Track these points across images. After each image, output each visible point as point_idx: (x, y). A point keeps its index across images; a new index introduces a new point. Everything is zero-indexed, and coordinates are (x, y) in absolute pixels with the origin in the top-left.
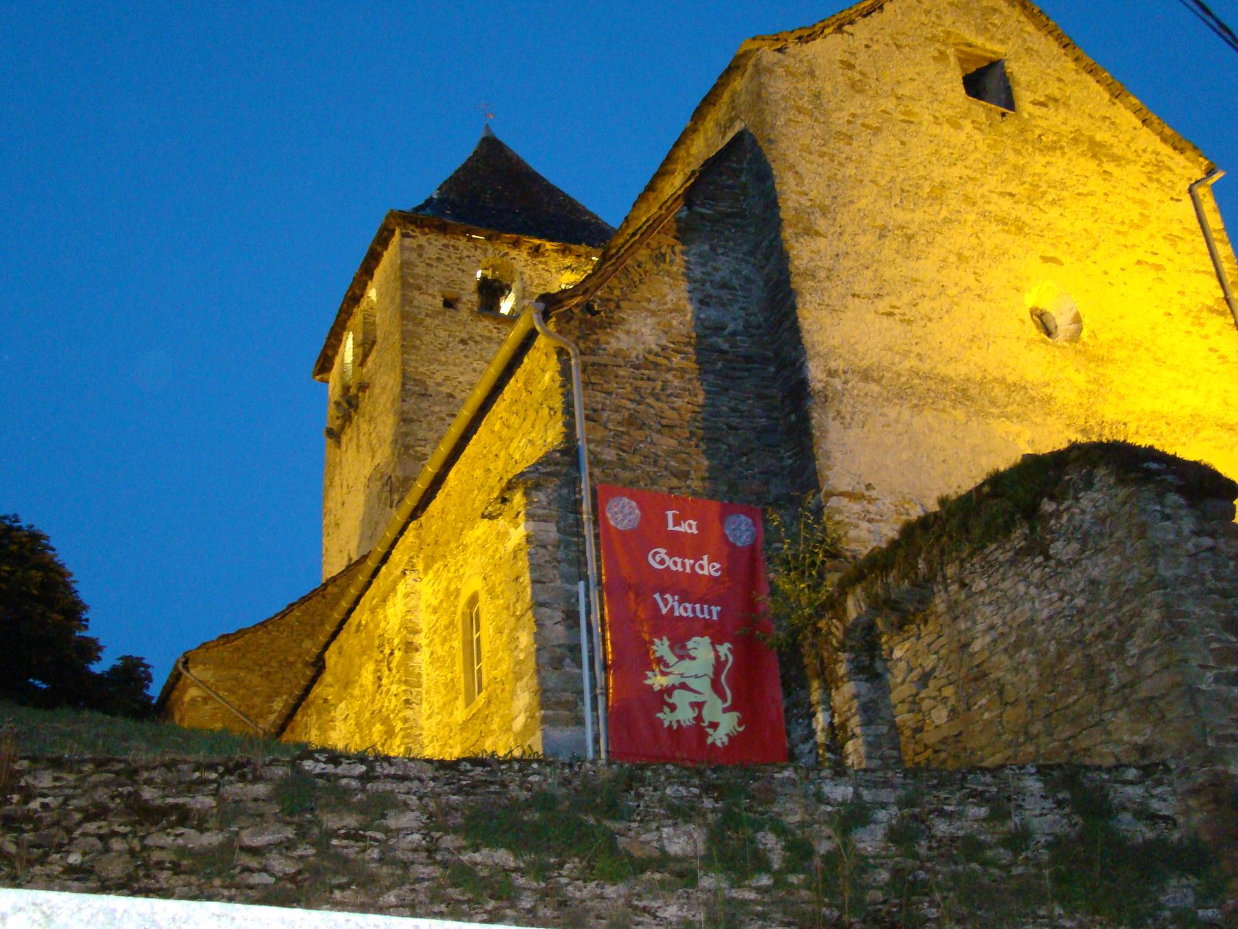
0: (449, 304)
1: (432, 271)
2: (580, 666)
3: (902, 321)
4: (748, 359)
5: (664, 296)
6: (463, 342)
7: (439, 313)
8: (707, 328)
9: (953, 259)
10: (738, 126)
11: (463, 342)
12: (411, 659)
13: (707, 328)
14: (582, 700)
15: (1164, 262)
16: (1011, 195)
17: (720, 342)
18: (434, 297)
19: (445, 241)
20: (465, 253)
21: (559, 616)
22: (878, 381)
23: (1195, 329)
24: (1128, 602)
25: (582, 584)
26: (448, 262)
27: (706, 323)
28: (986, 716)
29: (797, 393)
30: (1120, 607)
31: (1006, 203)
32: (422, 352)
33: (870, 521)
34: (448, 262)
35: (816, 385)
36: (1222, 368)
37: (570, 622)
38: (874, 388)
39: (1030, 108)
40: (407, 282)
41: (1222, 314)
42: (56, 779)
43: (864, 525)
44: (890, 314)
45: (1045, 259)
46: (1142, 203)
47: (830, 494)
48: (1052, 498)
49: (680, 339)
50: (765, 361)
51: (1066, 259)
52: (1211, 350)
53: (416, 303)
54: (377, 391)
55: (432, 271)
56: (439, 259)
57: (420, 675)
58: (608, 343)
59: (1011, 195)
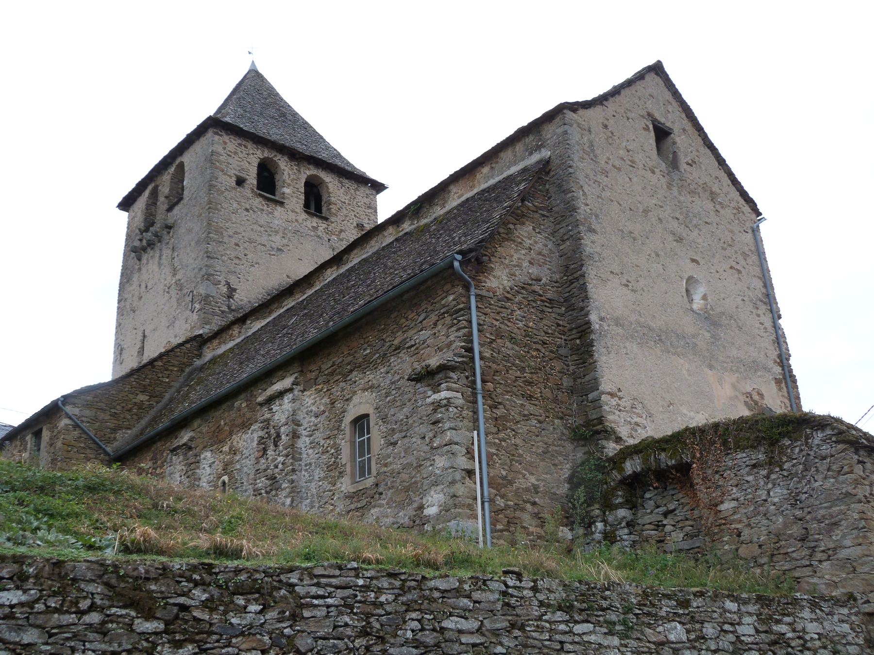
0: (240, 182)
1: (231, 161)
2: (475, 483)
3: (632, 290)
4: (551, 301)
5: (512, 256)
6: (247, 210)
7: (234, 188)
8: (532, 280)
9: (653, 255)
10: (545, 153)
11: (247, 210)
12: (296, 443)
13: (532, 280)
14: (476, 504)
15: (742, 269)
16: (678, 219)
17: (537, 288)
18: (231, 177)
19: (240, 142)
20: (251, 152)
21: (464, 451)
22: (622, 326)
23: (754, 311)
24: (836, 505)
25: (475, 432)
26: (241, 155)
27: (532, 276)
28: (726, 547)
29: (584, 330)
30: (830, 507)
31: (675, 224)
32: (221, 213)
33: (620, 411)
34: (241, 155)
35: (596, 326)
36: (765, 335)
37: (468, 456)
38: (620, 330)
39: (685, 166)
40: (211, 159)
41: (765, 303)
42: (390, 583)
43: (617, 413)
44: (627, 286)
45: (693, 260)
46: (731, 231)
47: (603, 393)
48: (790, 438)
49: (520, 284)
50: (560, 304)
51: (702, 262)
52: (761, 323)
53: (219, 180)
54: (182, 230)
55: (231, 161)
56: (236, 153)
57: (300, 454)
58: (485, 282)
59: (678, 219)
